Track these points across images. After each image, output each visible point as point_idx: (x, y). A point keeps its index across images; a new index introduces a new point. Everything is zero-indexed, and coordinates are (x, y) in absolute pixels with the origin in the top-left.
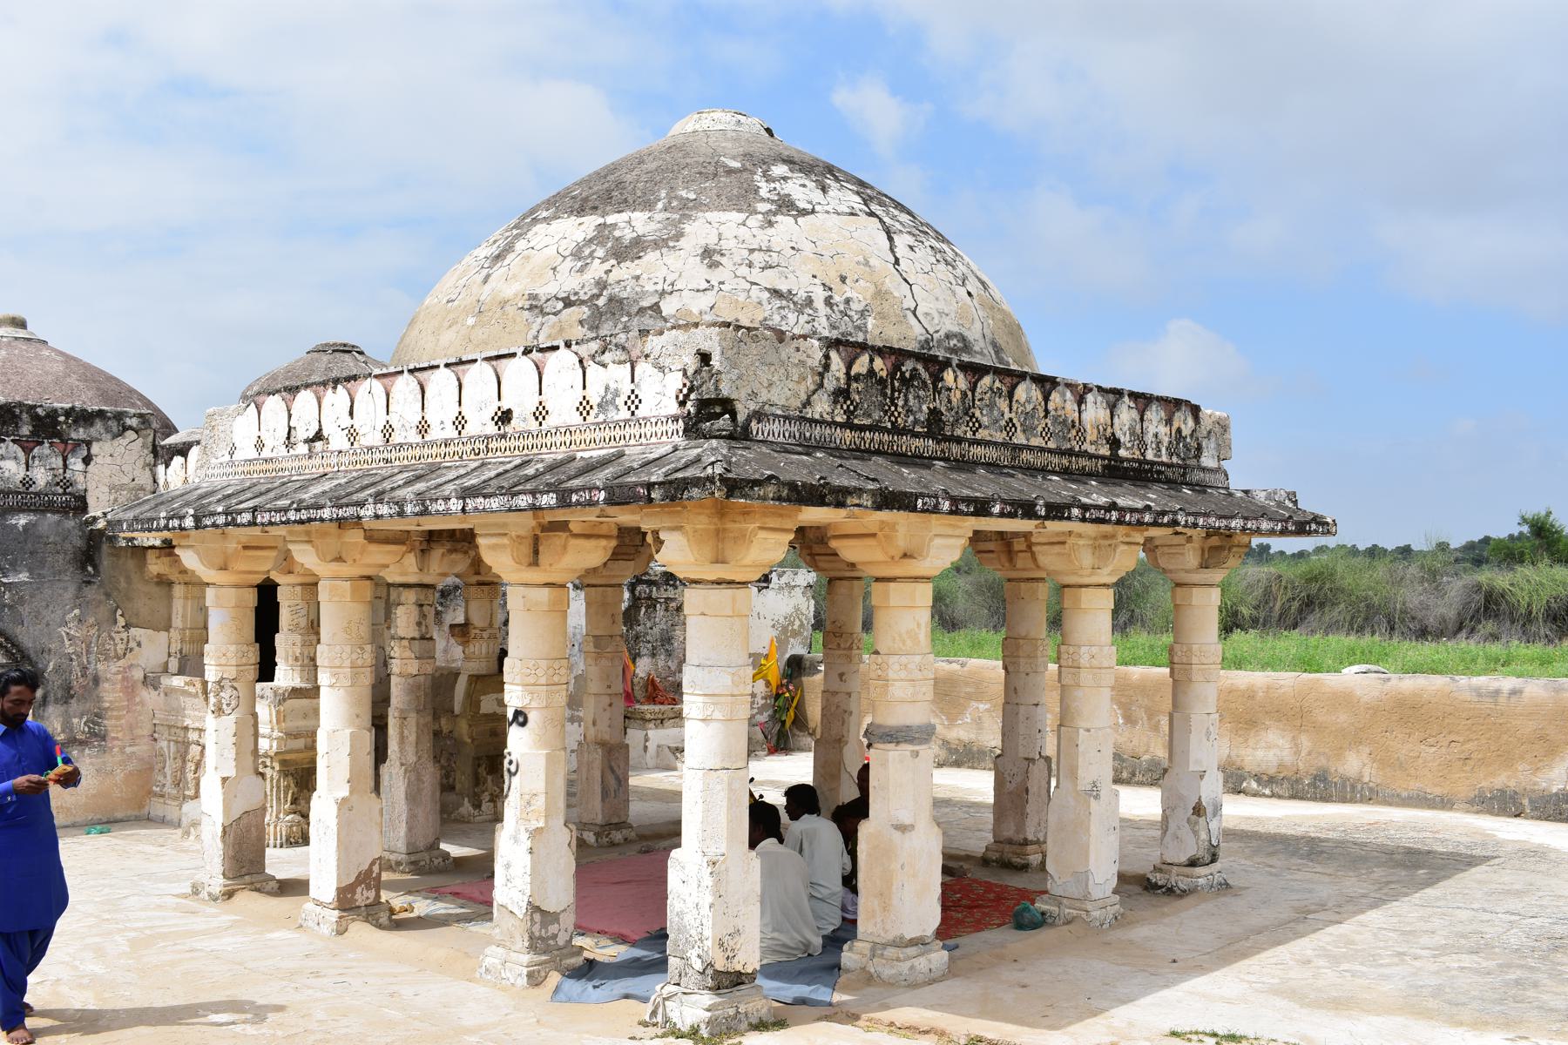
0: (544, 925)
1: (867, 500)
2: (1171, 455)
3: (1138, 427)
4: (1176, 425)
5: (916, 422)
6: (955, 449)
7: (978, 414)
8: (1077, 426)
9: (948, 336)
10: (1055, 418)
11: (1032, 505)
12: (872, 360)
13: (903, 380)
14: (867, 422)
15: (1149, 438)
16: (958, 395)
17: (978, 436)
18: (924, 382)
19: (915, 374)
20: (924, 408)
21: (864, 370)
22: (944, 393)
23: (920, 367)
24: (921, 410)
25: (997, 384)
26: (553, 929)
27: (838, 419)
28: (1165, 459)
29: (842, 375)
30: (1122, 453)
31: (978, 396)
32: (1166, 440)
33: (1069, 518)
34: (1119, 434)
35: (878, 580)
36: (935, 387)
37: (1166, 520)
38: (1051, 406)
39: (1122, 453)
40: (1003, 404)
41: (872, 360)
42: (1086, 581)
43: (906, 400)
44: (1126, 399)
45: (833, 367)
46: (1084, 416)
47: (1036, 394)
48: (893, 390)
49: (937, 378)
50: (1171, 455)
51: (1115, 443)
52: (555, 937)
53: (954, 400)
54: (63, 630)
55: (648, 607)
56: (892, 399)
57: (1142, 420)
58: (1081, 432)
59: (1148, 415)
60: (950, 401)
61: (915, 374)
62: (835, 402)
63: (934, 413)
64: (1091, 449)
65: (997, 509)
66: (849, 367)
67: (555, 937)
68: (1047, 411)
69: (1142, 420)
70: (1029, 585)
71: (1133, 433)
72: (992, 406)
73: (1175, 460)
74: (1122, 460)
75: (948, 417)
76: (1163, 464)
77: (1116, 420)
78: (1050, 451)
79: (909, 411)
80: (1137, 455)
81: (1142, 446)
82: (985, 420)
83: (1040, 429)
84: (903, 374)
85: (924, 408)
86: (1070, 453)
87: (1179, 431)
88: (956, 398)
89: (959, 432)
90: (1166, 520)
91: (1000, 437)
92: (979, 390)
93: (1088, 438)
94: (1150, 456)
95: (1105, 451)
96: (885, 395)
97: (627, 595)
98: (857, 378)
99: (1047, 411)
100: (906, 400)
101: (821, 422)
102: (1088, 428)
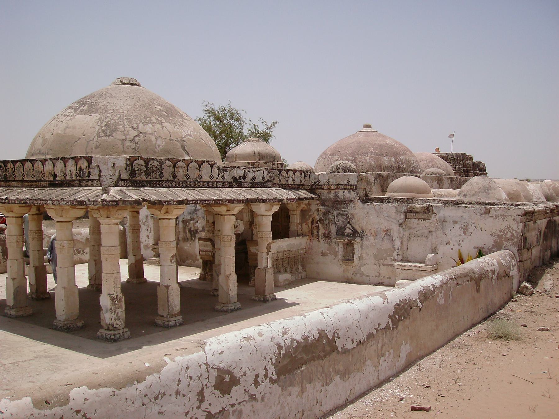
2: (77, 177)
6: (8, 184)
8: (42, 173)
11: (123, 203)
15: (68, 172)
28: (74, 179)
30: (57, 178)
32: (75, 172)
35: (222, 215)
49: (6, 166)
51: (55, 176)
57: (65, 166)
58: (43, 174)
59: (67, 164)
69: (65, 166)
70: (167, 221)
71: (62, 171)
73: (78, 178)
75: (8, 175)
76: (73, 181)
81: (65, 175)
89: (11, 179)
91: (21, 179)
94: (68, 178)
95: (51, 178)
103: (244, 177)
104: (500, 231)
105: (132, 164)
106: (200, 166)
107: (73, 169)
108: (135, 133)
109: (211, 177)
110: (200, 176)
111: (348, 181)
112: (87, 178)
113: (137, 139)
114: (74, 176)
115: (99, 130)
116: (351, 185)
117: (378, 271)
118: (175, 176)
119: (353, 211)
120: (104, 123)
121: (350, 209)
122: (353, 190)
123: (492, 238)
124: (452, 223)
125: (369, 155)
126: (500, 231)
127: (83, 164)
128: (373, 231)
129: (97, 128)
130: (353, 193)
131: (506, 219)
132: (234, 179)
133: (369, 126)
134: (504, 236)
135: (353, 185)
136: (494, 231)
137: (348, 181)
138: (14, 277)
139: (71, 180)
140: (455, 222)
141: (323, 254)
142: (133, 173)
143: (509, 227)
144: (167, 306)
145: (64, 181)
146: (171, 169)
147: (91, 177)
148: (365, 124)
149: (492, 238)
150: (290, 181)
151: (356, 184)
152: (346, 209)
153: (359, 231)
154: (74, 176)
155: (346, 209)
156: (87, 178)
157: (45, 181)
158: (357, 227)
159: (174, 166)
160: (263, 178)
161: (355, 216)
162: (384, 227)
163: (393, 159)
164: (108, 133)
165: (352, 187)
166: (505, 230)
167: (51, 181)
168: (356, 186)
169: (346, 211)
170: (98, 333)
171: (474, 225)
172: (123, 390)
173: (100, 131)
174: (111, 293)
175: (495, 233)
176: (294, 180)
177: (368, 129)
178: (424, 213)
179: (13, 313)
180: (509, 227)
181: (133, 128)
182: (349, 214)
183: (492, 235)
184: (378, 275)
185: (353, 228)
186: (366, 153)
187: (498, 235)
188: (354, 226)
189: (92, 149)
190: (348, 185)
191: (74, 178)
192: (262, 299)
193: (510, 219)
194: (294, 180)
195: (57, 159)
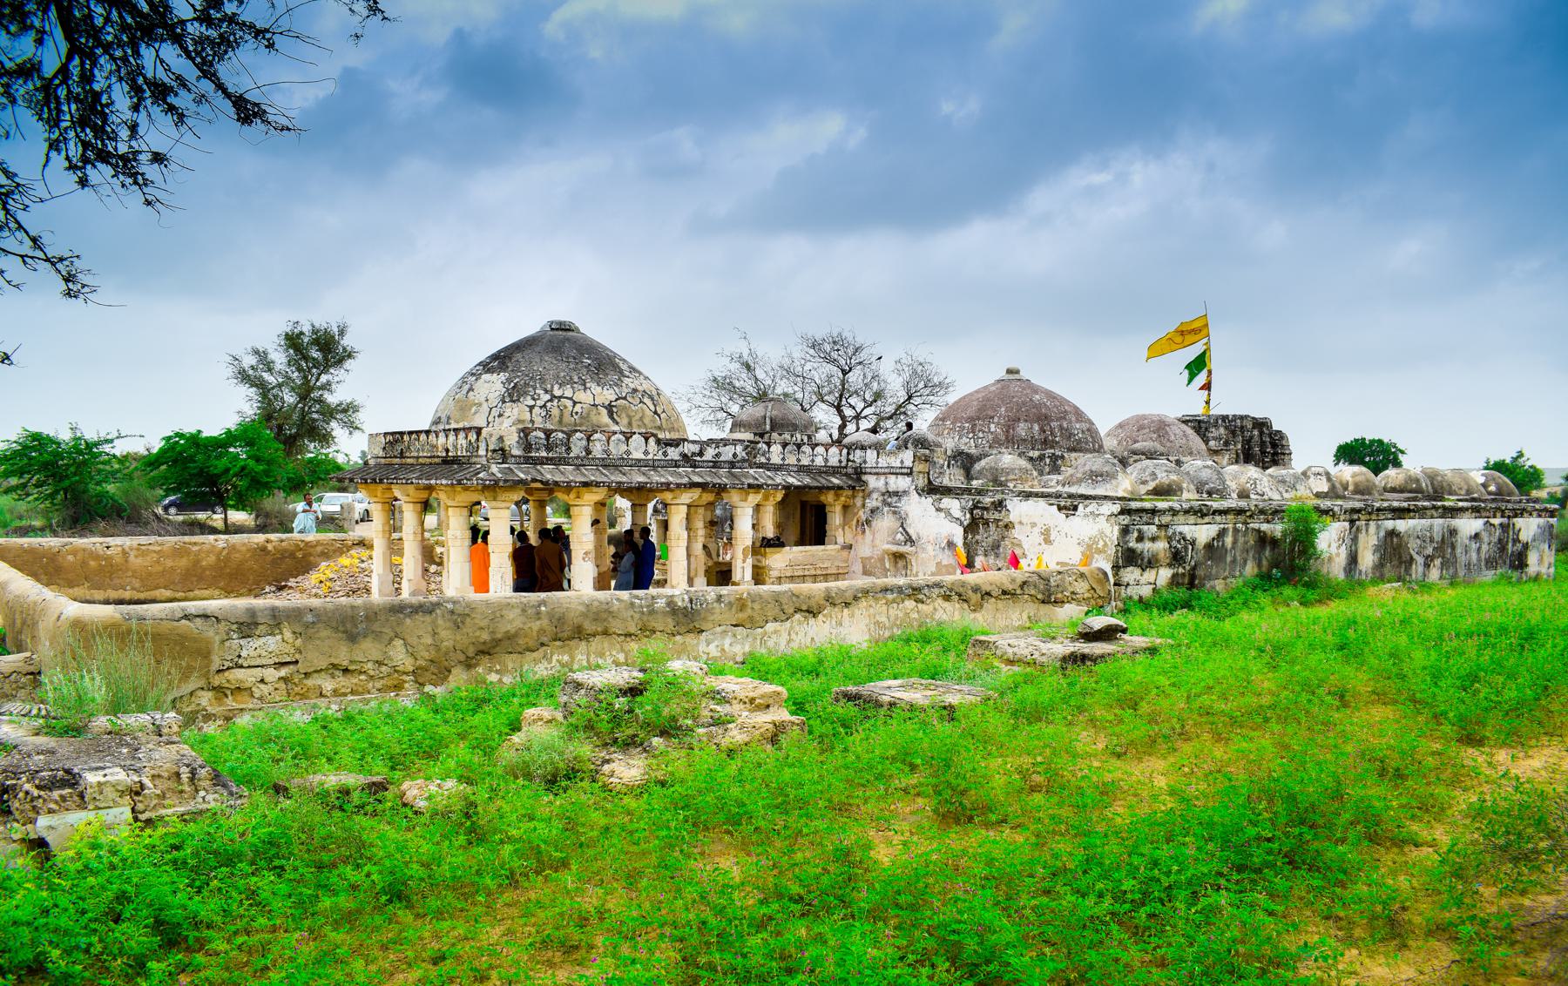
51: (447, 451)
103: (701, 454)
105: (526, 436)
106: (627, 439)
109: (646, 453)
110: (628, 453)
118: (588, 452)
127: (473, 437)
132: (684, 456)
133: (1017, 372)
140: (1034, 525)
141: (909, 426)
142: (528, 447)
143: (1102, 533)
146: (584, 442)
150: (819, 461)
158: (911, 531)
159: (588, 439)
160: (735, 455)
163: (1036, 427)
172: (750, 511)
176: (826, 460)
177: (1011, 377)
180: (1102, 533)
193: (1102, 519)
194: (826, 460)
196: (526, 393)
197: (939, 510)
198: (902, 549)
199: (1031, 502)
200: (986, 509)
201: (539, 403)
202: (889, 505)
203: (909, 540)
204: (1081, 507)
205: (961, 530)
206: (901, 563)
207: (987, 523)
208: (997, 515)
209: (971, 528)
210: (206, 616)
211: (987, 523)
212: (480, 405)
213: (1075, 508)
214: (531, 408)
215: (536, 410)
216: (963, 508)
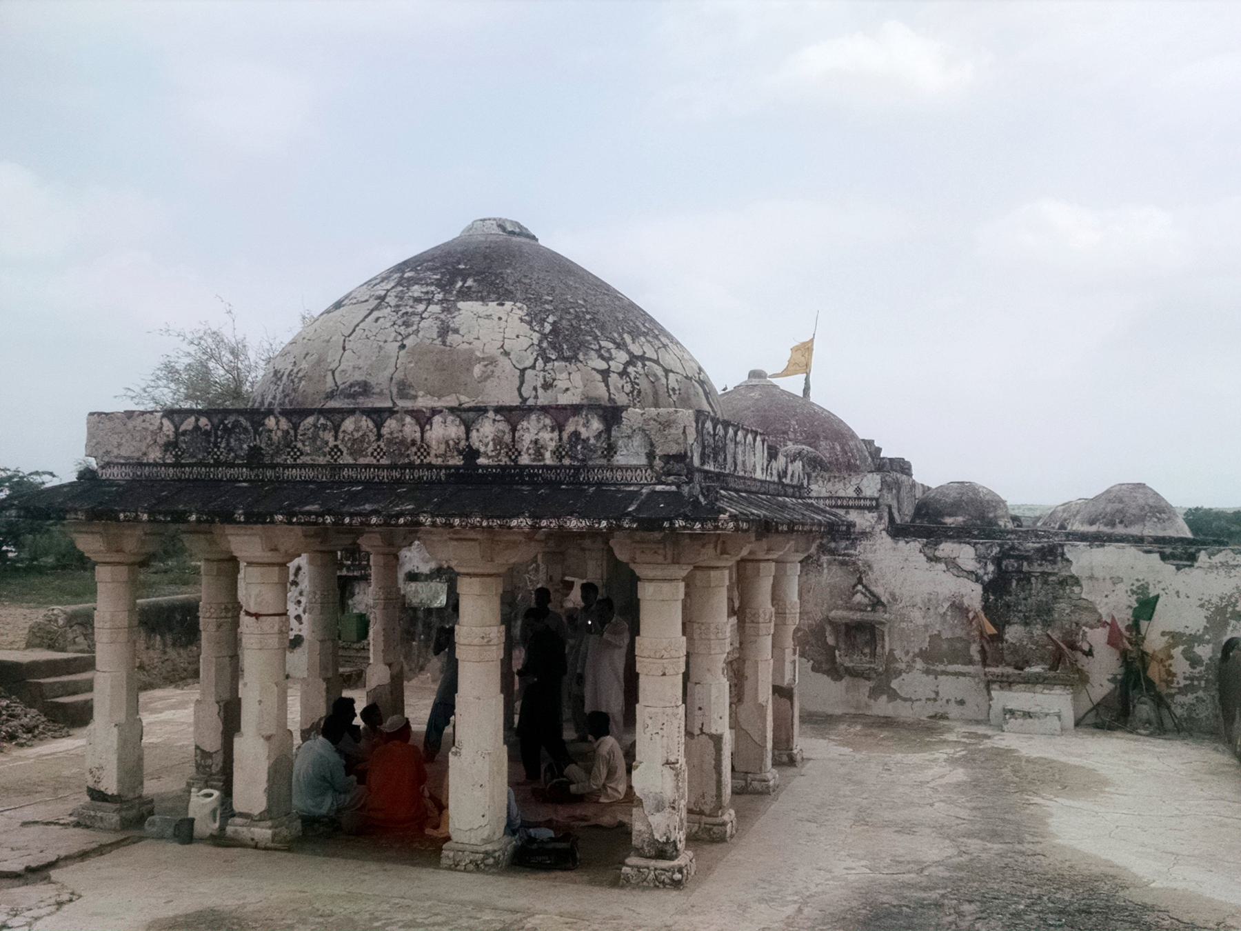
0: (202, 758)
1: (81, 516)
2: (561, 458)
3: (507, 438)
4: (570, 428)
5: (237, 457)
7: (299, 445)
9: (351, 386)
10: (390, 442)
12: (197, 420)
13: (226, 429)
14: (194, 460)
16: (280, 433)
17: (298, 461)
18: (246, 429)
19: (236, 424)
20: (245, 446)
21: (190, 428)
22: (265, 435)
23: (242, 419)
24: (241, 449)
25: (322, 421)
26: (209, 762)
27: (168, 461)
29: (171, 433)
30: (482, 461)
31: (300, 432)
32: (552, 445)
33: (272, 522)
34: (476, 444)
36: (256, 432)
37: (402, 521)
38: (385, 431)
39: (482, 461)
40: (329, 436)
41: (197, 420)
42: (704, 564)
43: (228, 443)
44: (491, 414)
45: (165, 429)
46: (427, 435)
47: (366, 423)
48: (217, 437)
50: (561, 458)
51: (471, 454)
52: (210, 767)
53: (275, 438)
54: (526, 576)
55: (1019, 581)
56: (216, 445)
60: (270, 439)
61: (236, 424)
62: (166, 451)
63: (255, 452)
64: (434, 461)
65: (193, 518)
66: (177, 428)
67: (210, 767)
68: (379, 436)
69: (514, 430)
72: (314, 438)
73: (567, 462)
74: (486, 467)
77: (474, 434)
78: (383, 467)
79: (231, 450)
80: (504, 460)
81: (513, 449)
82: (308, 449)
83: (370, 450)
84: (225, 426)
85: (245, 446)
86: (411, 466)
87: (576, 434)
88: (277, 436)
90: (402, 521)
92: (301, 428)
93: (433, 453)
94: (525, 460)
95: (457, 461)
96: (209, 442)
97: (991, 568)
98: (184, 433)
99: (379, 436)
100: (228, 443)
101: (156, 464)
102: (434, 444)
104: (1221, 599)
107: (549, 438)
108: (622, 357)
111: (858, 490)
112: (604, 462)
113: (631, 369)
114: (548, 455)
115: (540, 341)
116: (865, 499)
117: (934, 688)
119: (870, 556)
120: (548, 328)
121: (863, 552)
122: (870, 509)
123: (1203, 613)
124: (1109, 582)
125: (792, 436)
126: (1221, 599)
128: (918, 600)
129: (536, 336)
130: (870, 517)
131: (1233, 572)
134: (1230, 609)
135: (871, 499)
136: (1206, 598)
137: (858, 490)
138: (269, 733)
139: (538, 467)
140: (1116, 580)
144: (713, 784)
145: (504, 468)
147: (619, 459)
148: (753, 368)
149: (1203, 613)
151: (876, 495)
152: (852, 552)
153: (884, 599)
154: (548, 455)
155: (852, 552)
156: (604, 462)
157: (430, 467)
158: (878, 590)
161: (875, 567)
162: (947, 592)
164: (567, 354)
165: (868, 503)
166: (1231, 596)
167: (457, 468)
168: (877, 500)
169: (848, 555)
170: (625, 869)
171: (1161, 586)
173: (545, 345)
174: (672, 759)
175: (1209, 601)
177: (755, 381)
178: (1044, 558)
179: (263, 833)
181: (614, 342)
182: (860, 563)
183: (1202, 606)
184: (933, 696)
185: (871, 592)
186: (785, 433)
187: (1217, 607)
188: (873, 588)
189: (535, 389)
190: (859, 499)
191: (549, 459)
192: (785, 759)
195: (481, 410)
196: (583, 345)
197: (933, 559)
198: (869, 616)
199: (1111, 548)
200: (1027, 558)
201: (616, 366)
202: (832, 552)
203: (876, 603)
204: (1203, 556)
205: (978, 588)
206: (861, 638)
207: (1026, 578)
208: (1048, 568)
209: (995, 587)
210: (495, 909)
211: (1026, 578)
212: (492, 361)
213: (1192, 558)
214: (605, 374)
215: (614, 378)
216: (980, 558)
